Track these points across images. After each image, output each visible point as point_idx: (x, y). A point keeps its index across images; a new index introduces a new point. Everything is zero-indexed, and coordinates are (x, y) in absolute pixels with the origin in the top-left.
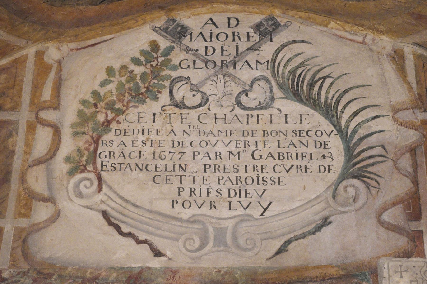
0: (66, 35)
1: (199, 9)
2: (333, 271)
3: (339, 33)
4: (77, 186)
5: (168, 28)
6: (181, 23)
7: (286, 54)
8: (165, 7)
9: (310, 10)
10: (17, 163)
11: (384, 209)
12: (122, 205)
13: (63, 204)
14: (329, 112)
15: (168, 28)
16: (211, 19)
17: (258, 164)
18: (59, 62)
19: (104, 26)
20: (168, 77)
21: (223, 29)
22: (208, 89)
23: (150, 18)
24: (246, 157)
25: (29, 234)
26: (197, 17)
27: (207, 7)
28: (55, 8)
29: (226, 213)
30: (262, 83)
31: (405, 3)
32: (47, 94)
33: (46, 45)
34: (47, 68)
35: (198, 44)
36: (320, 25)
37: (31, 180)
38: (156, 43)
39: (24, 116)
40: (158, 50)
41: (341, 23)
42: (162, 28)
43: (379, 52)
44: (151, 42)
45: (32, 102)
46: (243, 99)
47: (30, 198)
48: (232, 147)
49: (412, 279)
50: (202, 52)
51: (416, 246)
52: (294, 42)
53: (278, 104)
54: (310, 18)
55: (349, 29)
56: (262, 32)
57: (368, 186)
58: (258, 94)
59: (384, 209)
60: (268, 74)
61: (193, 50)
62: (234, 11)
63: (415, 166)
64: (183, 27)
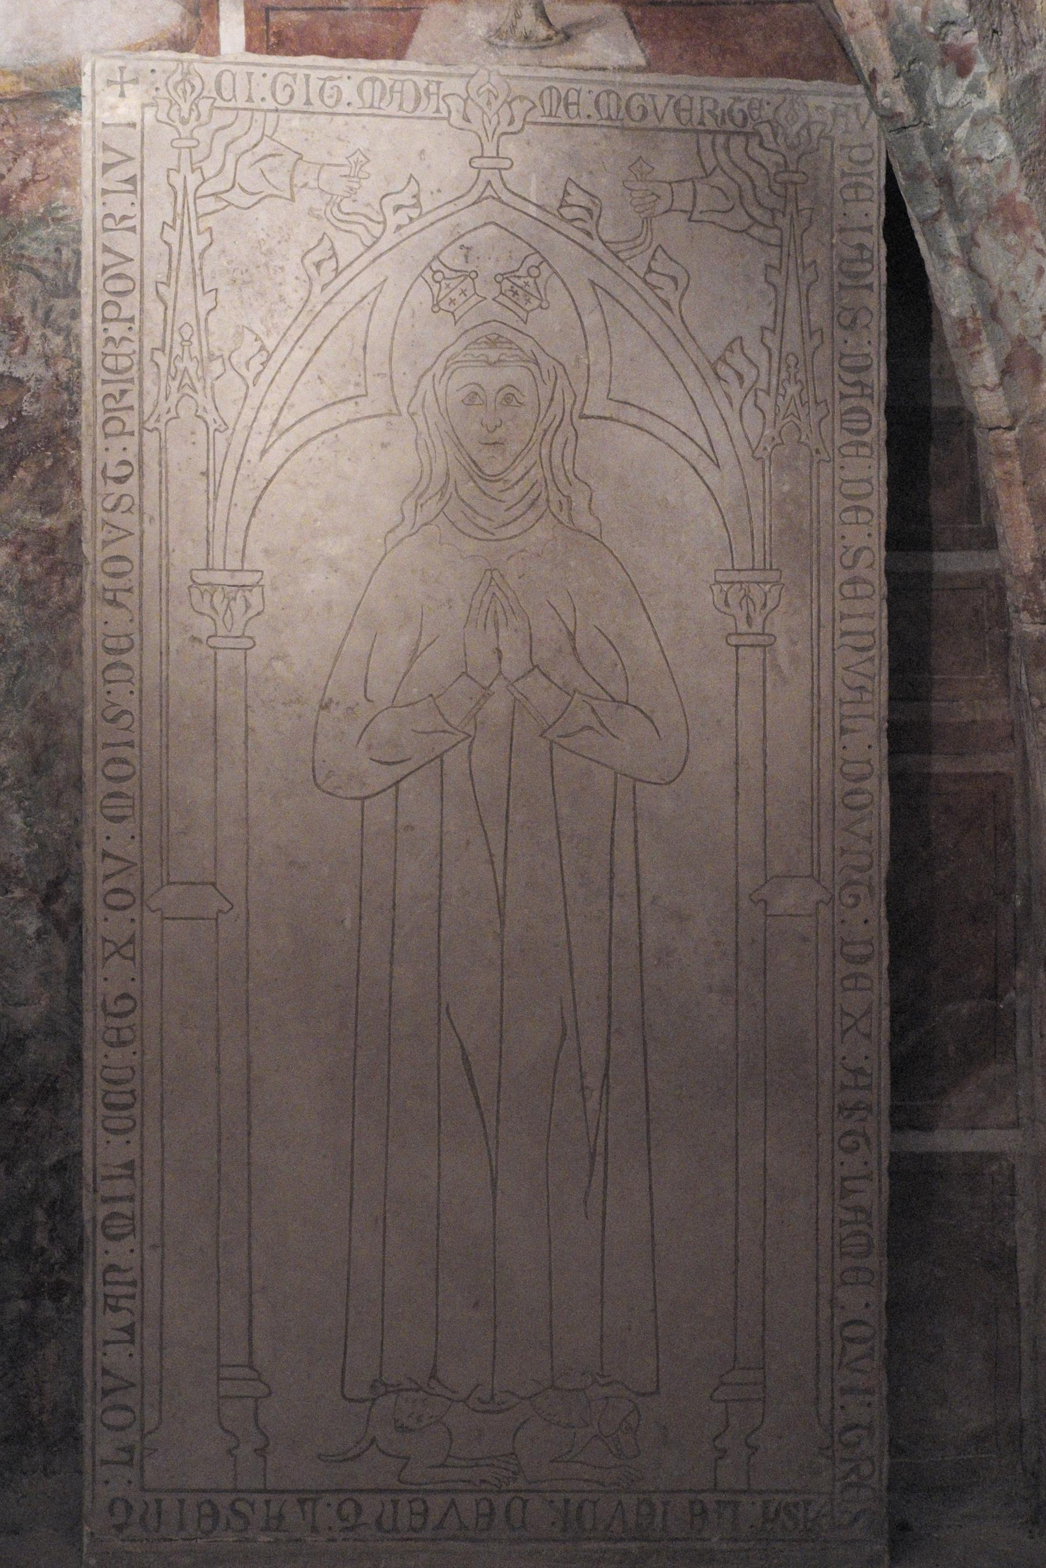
12: (574, 950)
49: (147, 101)
51: (200, 26)
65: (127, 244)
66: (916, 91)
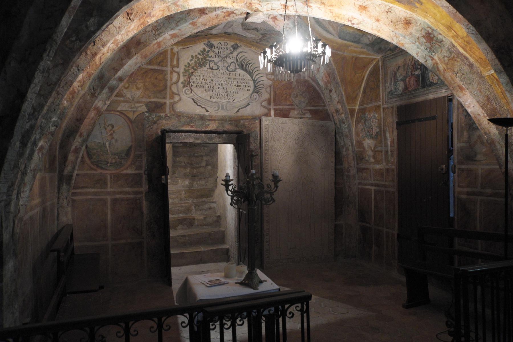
2: (250, 117)
4: (185, 91)
7: (240, 56)
10: (169, 83)
11: (263, 102)
13: (182, 96)
14: (250, 74)
17: (232, 87)
18: (178, 52)
20: (208, 60)
21: (223, 46)
22: (219, 64)
24: (229, 86)
25: (173, 104)
29: (224, 101)
30: (233, 64)
32: (175, 63)
34: (174, 54)
35: (216, 50)
37: (173, 88)
39: (169, 69)
45: (171, 65)
46: (228, 68)
47: (173, 94)
48: (225, 82)
50: (217, 53)
53: (237, 70)
57: (259, 95)
58: (232, 67)
59: (263, 102)
60: (235, 61)
63: (271, 91)
65: (267, 136)
66: (340, 125)
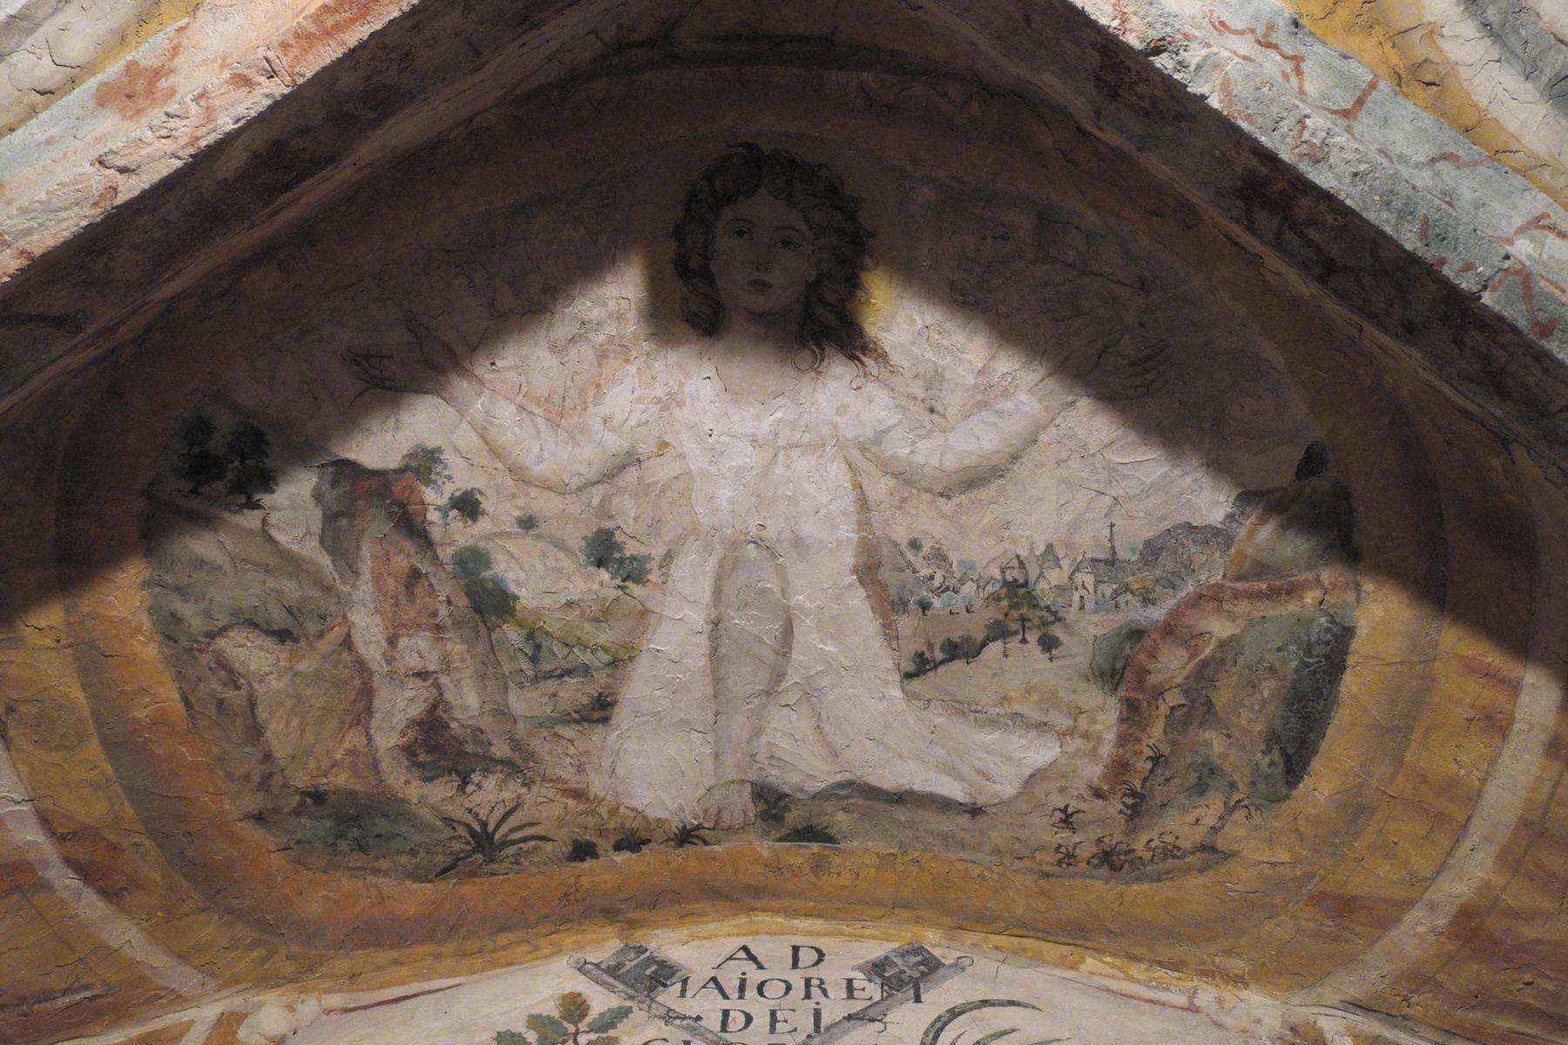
0: (324, 969)
1: (712, 926)
3: (1115, 985)
5: (619, 966)
6: (660, 956)
8: (618, 912)
9: (1023, 928)
15: (619, 966)
16: (745, 949)
19: (439, 956)
23: (575, 942)
26: (707, 943)
27: (737, 922)
28: (307, 875)
31: (1293, 865)
33: (256, 999)
36: (1058, 966)
38: (579, 1000)
40: (583, 1015)
41: (1117, 962)
42: (603, 966)
43: (1244, 1031)
44: (564, 997)
50: (713, 1022)
52: (985, 1003)
54: (1024, 950)
55: (1142, 977)
56: (889, 979)
61: (685, 1018)
62: (810, 933)
64: (662, 964)
